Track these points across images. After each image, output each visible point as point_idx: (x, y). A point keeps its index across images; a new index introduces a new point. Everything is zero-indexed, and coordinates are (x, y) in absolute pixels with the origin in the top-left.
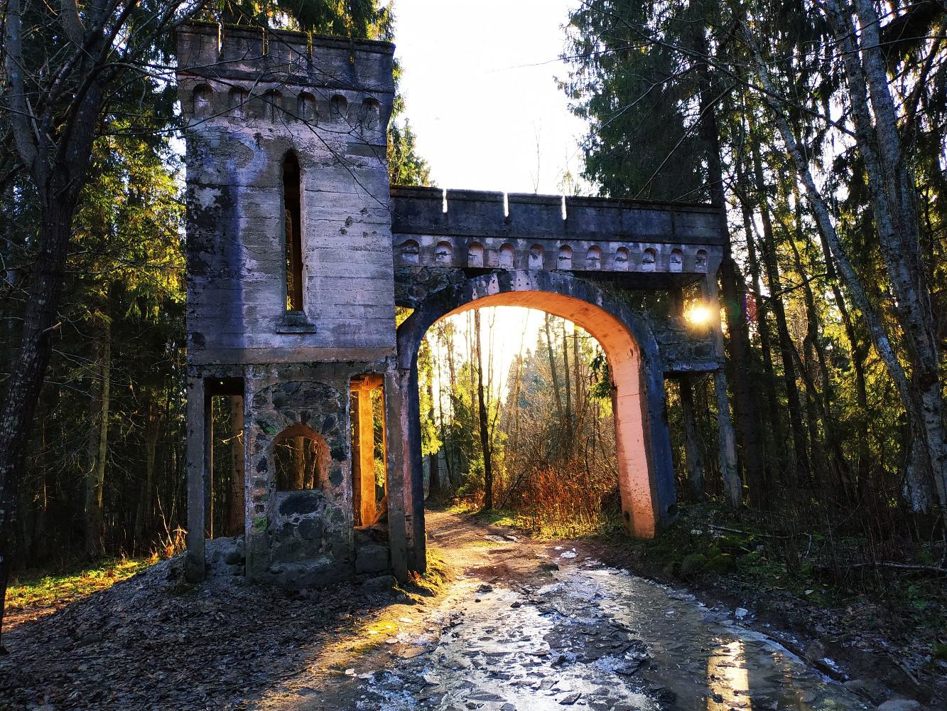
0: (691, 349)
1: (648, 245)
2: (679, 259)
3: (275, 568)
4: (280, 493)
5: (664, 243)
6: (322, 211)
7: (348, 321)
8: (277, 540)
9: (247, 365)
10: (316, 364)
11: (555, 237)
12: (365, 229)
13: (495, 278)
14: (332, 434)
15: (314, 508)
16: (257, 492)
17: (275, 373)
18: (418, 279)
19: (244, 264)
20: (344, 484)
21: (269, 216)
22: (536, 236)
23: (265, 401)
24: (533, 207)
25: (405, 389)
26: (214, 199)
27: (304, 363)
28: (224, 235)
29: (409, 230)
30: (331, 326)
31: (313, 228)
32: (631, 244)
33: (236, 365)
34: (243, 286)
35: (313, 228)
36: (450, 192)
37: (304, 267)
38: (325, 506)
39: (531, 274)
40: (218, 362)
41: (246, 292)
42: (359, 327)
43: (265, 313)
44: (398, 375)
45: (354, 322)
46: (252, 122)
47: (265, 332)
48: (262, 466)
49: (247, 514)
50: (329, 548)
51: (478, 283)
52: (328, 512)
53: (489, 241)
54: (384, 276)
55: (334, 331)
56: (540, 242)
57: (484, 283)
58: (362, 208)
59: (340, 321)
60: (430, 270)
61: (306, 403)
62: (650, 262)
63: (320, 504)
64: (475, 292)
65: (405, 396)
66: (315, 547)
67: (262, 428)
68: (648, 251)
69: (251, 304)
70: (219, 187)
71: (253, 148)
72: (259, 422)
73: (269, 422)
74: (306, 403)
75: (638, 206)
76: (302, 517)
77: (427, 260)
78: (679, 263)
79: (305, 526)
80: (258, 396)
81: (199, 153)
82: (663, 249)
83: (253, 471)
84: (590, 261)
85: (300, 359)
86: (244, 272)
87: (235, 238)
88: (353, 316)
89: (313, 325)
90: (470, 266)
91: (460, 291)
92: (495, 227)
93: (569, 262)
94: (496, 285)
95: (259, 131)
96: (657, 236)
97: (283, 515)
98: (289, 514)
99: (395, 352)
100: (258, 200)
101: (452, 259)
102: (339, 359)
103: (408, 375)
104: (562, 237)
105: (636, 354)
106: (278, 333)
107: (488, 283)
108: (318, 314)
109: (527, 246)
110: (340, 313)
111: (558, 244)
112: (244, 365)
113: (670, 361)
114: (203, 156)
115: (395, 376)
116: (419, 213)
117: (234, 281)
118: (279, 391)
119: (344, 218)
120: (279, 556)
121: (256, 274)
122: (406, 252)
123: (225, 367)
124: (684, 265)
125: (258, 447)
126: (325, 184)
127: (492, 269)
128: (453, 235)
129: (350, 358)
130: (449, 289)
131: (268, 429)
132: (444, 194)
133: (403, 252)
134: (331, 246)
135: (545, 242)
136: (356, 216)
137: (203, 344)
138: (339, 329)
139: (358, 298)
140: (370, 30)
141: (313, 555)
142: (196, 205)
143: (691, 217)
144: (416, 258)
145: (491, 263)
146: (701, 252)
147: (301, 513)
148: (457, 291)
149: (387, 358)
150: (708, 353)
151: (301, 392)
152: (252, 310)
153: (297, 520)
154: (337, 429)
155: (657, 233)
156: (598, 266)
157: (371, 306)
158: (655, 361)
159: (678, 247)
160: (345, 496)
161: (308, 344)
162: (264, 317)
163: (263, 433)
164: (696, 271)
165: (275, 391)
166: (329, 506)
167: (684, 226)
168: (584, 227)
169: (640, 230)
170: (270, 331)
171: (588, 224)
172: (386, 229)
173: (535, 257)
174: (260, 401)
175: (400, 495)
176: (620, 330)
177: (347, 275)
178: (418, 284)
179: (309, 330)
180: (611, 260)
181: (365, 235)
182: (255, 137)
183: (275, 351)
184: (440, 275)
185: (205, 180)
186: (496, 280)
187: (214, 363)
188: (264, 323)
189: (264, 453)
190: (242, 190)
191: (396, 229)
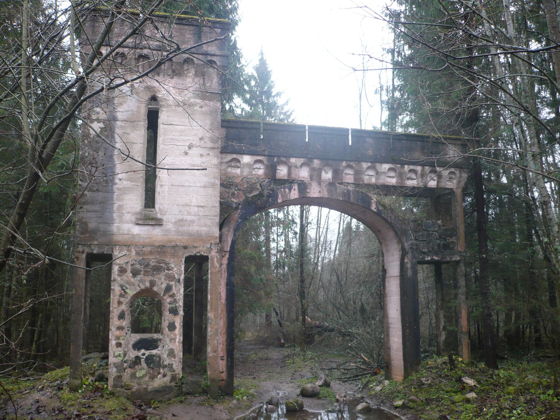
1: (412, 167)
4: (133, 335)
6: (172, 139)
7: (185, 217)
12: (202, 151)
13: (296, 187)
15: (156, 347)
21: (135, 141)
25: (224, 266)
28: (105, 154)
30: (173, 220)
31: (165, 151)
32: (399, 166)
34: (115, 190)
35: (165, 151)
36: (351, 129)
37: (158, 178)
38: (164, 346)
39: (323, 185)
41: (117, 195)
42: (192, 222)
43: (129, 210)
44: (219, 257)
45: (189, 218)
47: (128, 223)
51: (282, 190)
53: (293, 160)
54: (213, 185)
55: (175, 223)
57: (287, 190)
58: (200, 137)
59: (180, 217)
62: (413, 179)
63: (161, 345)
64: (280, 197)
65: (225, 271)
67: (123, 289)
68: (411, 171)
69: (120, 203)
73: (128, 286)
76: (147, 353)
78: (434, 180)
80: (121, 267)
82: (423, 170)
84: (368, 177)
86: (117, 181)
87: (111, 157)
88: (189, 214)
93: (352, 177)
98: (139, 349)
99: (218, 241)
100: (128, 130)
101: (265, 173)
102: (178, 244)
106: (137, 224)
107: (290, 190)
108: (165, 212)
109: (320, 165)
110: (181, 211)
111: (344, 164)
115: (217, 258)
119: (188, 144)
121: (125, 183)
122: (232, 167)
124: (438, 182)
125: (120, 303)
126: (176, 120)
127: (294, 180)
130: (261, 195)
131: (127, 290)
132: (307, 128)
133: (229, 166)
134: (177, 163)
136: (196, 142)
138: (180, 222)
139: (194, 200)
144: (238, 171)
146: (451, 173)
147: (147, 349)
149: (211, 244)
152: (120, 207)
153: (144, 354)
154: (174, 294)
156: (373, 180)
157: (202, 207)
160: (177, 340)
162: (129, 213)
163: (123, 293)
164: (447, 187)
170: (132, 222)
173: (326, 172)
174: (122, 271)
177: (187, 184)
178: (239, 190)
179: (158, 222)
181: (202, 155)
186: (297, 188)
188: (127, 217)
189: (123, 307)
191: (224, 151)
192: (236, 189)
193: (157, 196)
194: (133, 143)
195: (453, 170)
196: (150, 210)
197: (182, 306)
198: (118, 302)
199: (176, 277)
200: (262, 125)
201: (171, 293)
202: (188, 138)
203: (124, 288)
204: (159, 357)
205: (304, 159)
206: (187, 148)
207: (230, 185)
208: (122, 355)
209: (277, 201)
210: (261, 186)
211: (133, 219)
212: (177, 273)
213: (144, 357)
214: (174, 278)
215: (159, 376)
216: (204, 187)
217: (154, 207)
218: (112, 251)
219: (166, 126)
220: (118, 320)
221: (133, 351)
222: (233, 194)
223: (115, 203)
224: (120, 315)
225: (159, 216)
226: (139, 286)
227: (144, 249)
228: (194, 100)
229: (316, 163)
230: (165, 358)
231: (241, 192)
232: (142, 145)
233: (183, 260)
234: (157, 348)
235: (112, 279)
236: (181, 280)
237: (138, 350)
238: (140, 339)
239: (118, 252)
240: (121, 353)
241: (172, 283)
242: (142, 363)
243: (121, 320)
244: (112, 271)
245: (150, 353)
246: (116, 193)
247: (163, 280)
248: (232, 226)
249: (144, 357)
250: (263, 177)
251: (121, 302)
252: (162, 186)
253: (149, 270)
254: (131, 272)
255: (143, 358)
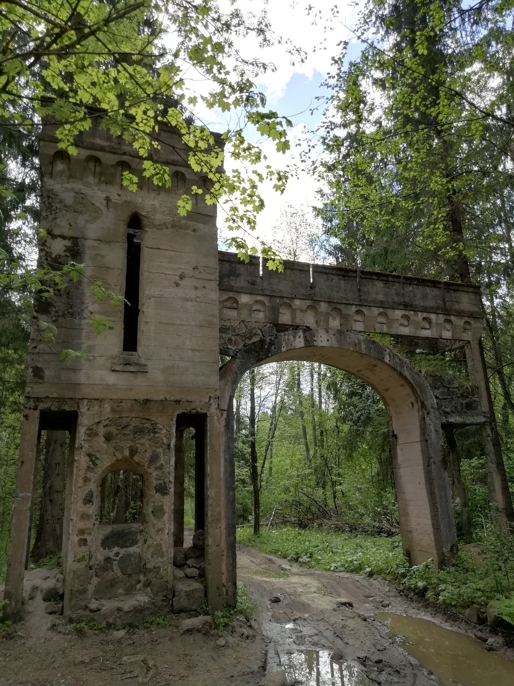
0: (462, 404)
1: (425, 315)
2: (448, 327)
3: (93, 605)
5: (437, 314)
8: (96, 576)
9: (82, 399)
10: (146, 401)
11: (351, 302)
13: (301, 333)
14: (157, 468)
15: (134, 543)
16: (81, 525)
17: (107, 407)
18: (237, 331)
19: (87, 307)
20: (166, 517)
22: (335, 301)
23: (97, 434)
24: (333, 277)
26: (64, 248)
27: (135, 400)
29: (230, 289)
33: (72, 399)
34: (84, 327)
37: (141, 313)
38: (146, 541)
39: (331, 332)
40: (55, 395)
46: (103, 186)
48: (88, 500)
49: (70, 547)
50: (147, 584)
51: (286, 337)
52: (149, 547)
53: (297, 302)
56: (339, 306)
57: (291, 338)
60: (247, 324)
61: (135, 438)
64: (284, 345)
66: (134, 582)
67: (91, 461)
69: (90, 343)
70: (70, 238)
71: (103, 208)
72: (89, 455)
73: (98, 456)
74: (135, 438)
75: (416, 283)
76: (123, 551)
77: (244, 315)
78: (449, 330)
79: (125, 560)
80: (90, 429)
81: (54, 208)
83: (80, 503)
85: (132, 395)
86: (86, 314)
89: (146, 365)
90: (280, 322)
91: (271, 343)
92: (303, 291)
94: (302, 340)
95: (108, 194)
96: (432, 308)
97: (104, 549)
102: (168, 398)
103: (225, 416)
104: (357, 303)
105: (416, 406)
107: (295, 337)
110: (171, 355)
112: (79, 399)
113: (446, 414)
114: (58, 211)
115: (217, 416)
116: (239, 275)
117: (76, 321)
118: (111, 425)
120: (100, 594)
123: (62, 400)
124: (454, 333)
125: (86, 480)
128: (267, 295)
129: (177, 397)
130: (262, 342)
131: (97, 462)
135: (343, 306)
137: (42, 378)
139: (188, 342)
140: (88, 294)
141: (130, 591)
142: (47, 252)
143: (458, 294)
145: (298, 322)
146: (466, 322)
147: (122, 547)
148: (269, 343)
150: (475, 408)
151: (131, 427)
153: (117, 554)
154: (162, 465)
155: (432, 305)
157: (198, 351)
158: (434, 413)
159: (448, 317)
161: (140, 381)
163: (92, 466)
165: (107, 425)
166: (150, 541)
167: (452, 301)
168: (374, 296)
169: (419, 302)
171: (377, 293)
172: (215, 285)
174: (92, 433)
175: (218, 531)
176: (402, 385)
177: (178, 322)
180: (396, 325)
181: (196, 288)
182: (105, 199)
183: (108, 387)
184: (255, 328)
185: (57, 231)
187: (51, 396)
190: (89, 243)
191: (223, 287)
192: (234, 333)
193: (139, 335)
194: (109, 268)
195: (468, 320)
196: (131, 353)
197: (173, 481)
198: (83, 478)
199: (165, 441)
200: (261, 260)
201: (158, 464)
202: (179, 266)
203: (94, 459)
204: (140, 557)
205: (310, 301)
206: (178, 277)
207: (226, 329)
208: (87, 557)
209: (281, 351)
210: (262, 332)
211: (109, 365)
212: (165, 437)
213: (118, 558)
214: (163, 443)
215: (139, 586)
216: (200, 326)
217: (135, 350)
218: (78, 407)
219: (152, 251)
220: (82, 505)
221: (102, 550)
222: (230, 340)
223: (84, 343)
224: (86, 497)
225: (143, 361)
226: (115, 455)
227: (122, 404)
228: (185, 221)
229: (323, 307)
230: (148, 559)
231: (238, 338)
232: (119, 271)
233: (175, 419)
234: (136, 543)
235: (76, 446)
236: (172, 446)
237: (109, 549)
238: (113, 531)
239: (87, 408)
240: (85, 554)
241: (160, 450)
242: (114, 568)
243: (87, 505)
244: (77, 434)
245: (125, 551)
246: (84, 330)
247: (148, 446)
248: (230, 379)
249: (118, 558)
250: (263, 321)
251: (88, 479)
252: (146, 323)
253: (128, 433)
254: (104, 436)
255: (116, 560)
